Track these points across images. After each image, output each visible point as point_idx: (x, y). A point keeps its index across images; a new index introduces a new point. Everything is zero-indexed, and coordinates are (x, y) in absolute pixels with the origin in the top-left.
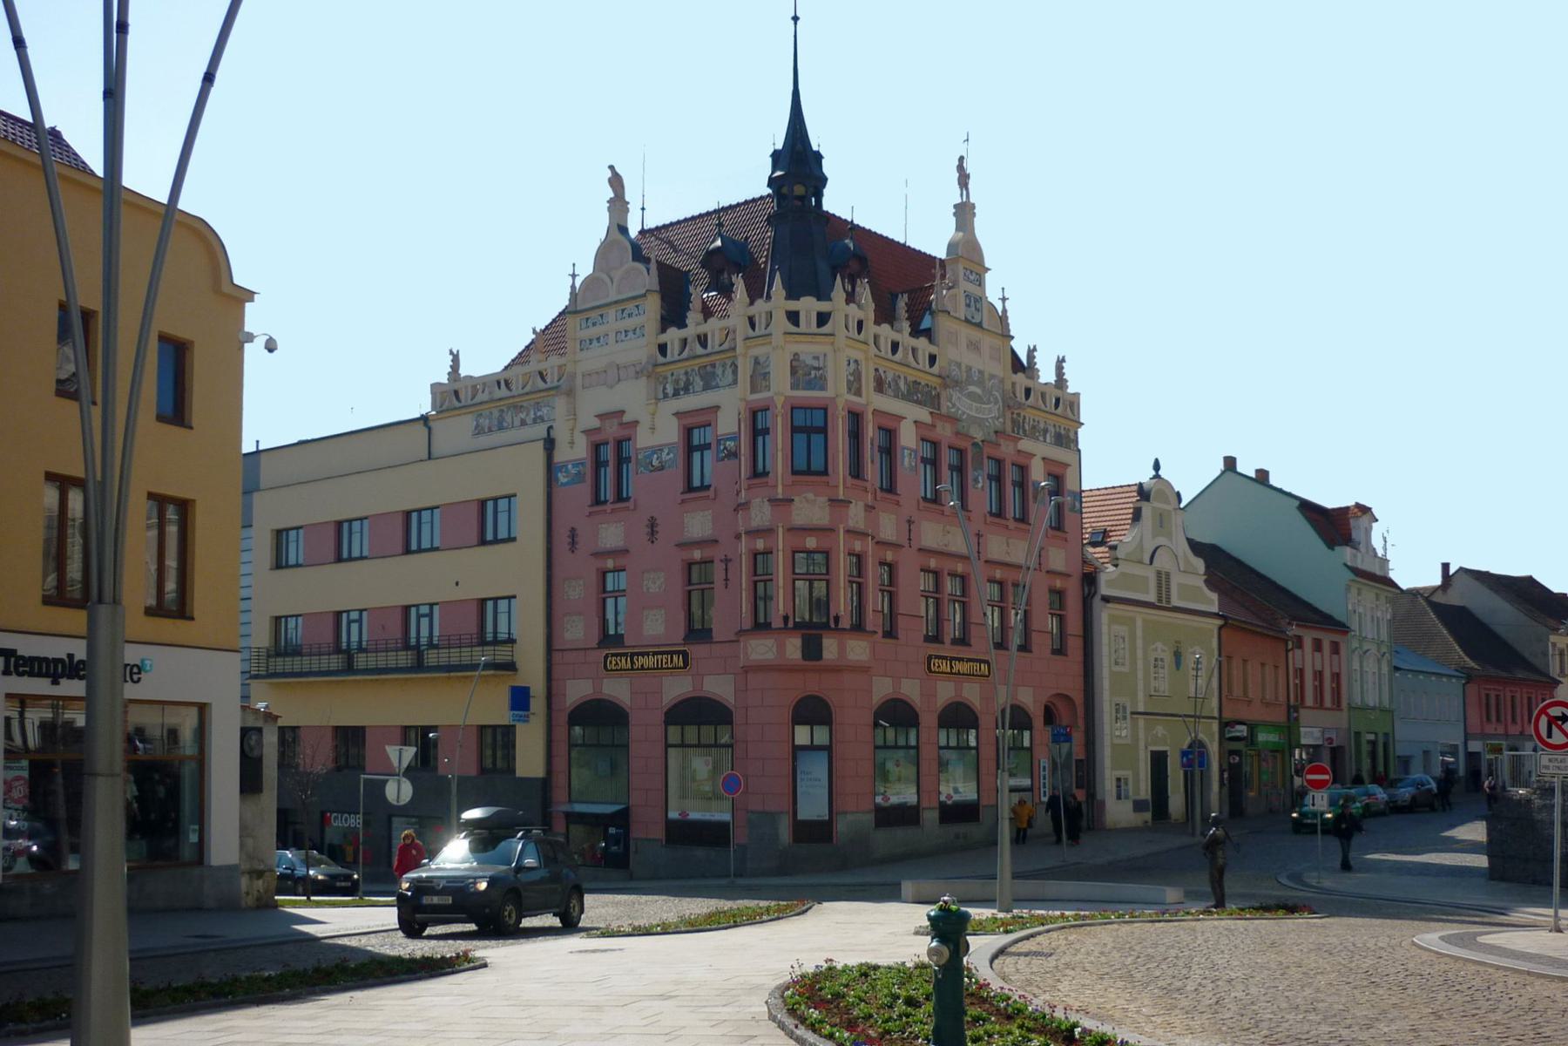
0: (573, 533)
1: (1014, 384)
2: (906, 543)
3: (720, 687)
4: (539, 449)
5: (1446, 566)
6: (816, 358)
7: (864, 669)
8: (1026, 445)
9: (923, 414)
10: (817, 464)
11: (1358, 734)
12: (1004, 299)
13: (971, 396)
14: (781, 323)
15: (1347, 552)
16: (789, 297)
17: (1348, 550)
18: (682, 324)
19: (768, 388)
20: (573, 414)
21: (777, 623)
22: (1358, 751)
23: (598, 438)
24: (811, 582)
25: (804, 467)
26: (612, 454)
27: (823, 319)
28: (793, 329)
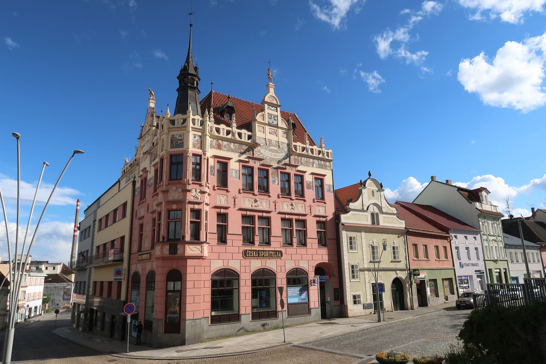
6: (180, 136)
8: (300, 168)
11: (490, 270)
15: (478, 205)
22: (89, 284)
24: (175, 222)
25: (175, 178)
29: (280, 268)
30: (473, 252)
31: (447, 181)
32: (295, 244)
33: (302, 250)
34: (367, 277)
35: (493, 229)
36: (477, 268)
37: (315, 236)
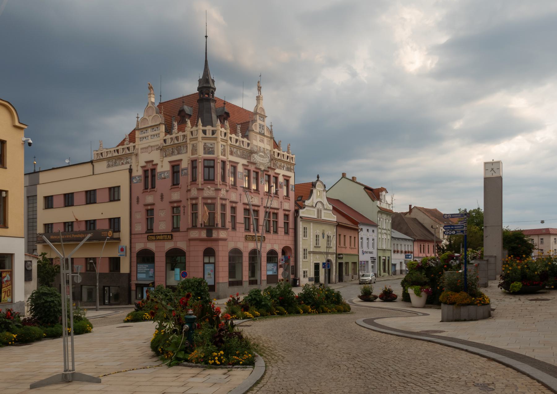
0: (138, 198)
1: (274, 152)
2: (239, 201)
3: (182, 245)
4: (127, 172)
5: (410, 206)
7: (225, 240)
8: (277, 171)
9: (245, 162)
10: (211, 178)
11: (380, 257)
12: (271, 126)
13: (260, 156)
14: (201, 134)
16: (203, 126)
17: (378, 202)
18: (197, 126)
19: (197, 154)
20: (137, 162)
21: (199, 226)
23: (146, 169)
26: (150, 174)
27: (213, 133)
28: (204, 136)
29: (265, 248)
30: (371, 242)
31: (353, 178)
32: (272, 232)
33: (275, 236)
34: (312, 258)
35: (385, 223)
36: (372, 255)
37: (243, 221)
